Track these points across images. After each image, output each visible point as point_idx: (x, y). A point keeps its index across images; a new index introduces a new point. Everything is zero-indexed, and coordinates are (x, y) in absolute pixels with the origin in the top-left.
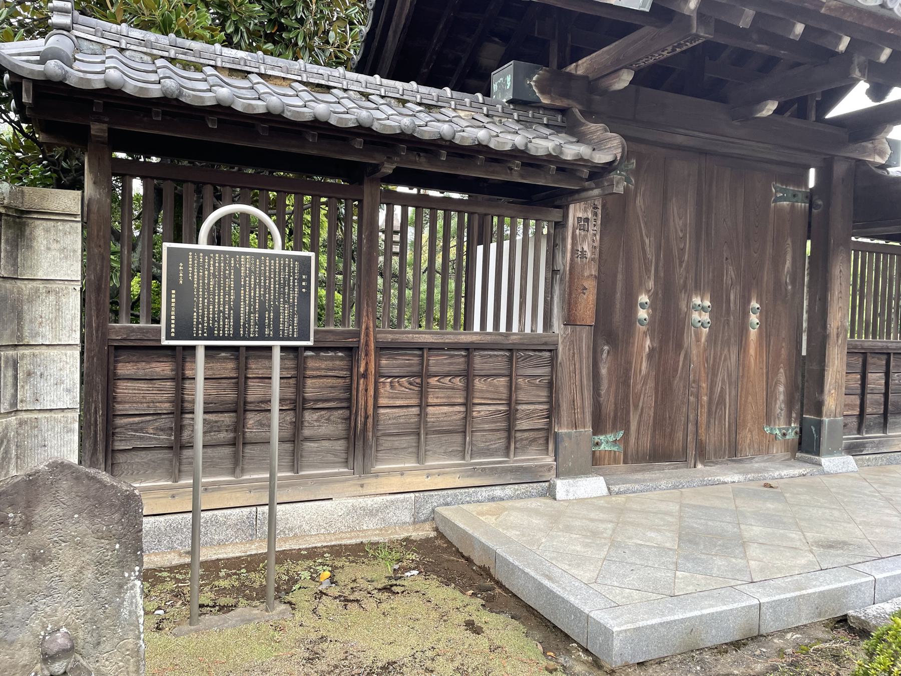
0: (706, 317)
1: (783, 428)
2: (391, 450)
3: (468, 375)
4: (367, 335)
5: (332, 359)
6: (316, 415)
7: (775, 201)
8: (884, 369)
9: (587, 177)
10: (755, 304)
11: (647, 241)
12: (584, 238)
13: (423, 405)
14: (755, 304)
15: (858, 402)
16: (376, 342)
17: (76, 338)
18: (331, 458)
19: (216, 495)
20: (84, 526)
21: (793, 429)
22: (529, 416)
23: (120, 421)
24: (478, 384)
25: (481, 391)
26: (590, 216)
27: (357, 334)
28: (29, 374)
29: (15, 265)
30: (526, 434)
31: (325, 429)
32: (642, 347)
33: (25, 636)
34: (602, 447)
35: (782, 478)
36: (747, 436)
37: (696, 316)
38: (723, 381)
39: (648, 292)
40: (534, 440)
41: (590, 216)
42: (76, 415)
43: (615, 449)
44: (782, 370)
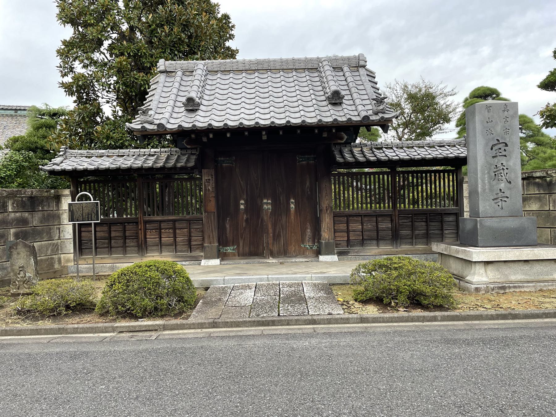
0: (270, 206)
2: (151, 250)
3: (175, 229)
4: (140, 218)
5: (132, 225)
6: (129, 241)
7: (299, 162)
8: (361, 222)
9: (361, 129)
11: (242, 183)
12: (209, 185)
13: (160, 238)
15: (346, 235)
16: (143, 220)
18: (134, 252)
19: (104, 260)
20: (24, 249)
21: (316, 246)
22: (196, 241)
23: (83, 242)
24: (177, 231)
25: (179, 233)
26: (210, 178)
28: (62, 231)
29: (58, 207)
30: (195, 246)
31: (132, 244)
32: (243, 217)
33: (17, 265)
34: (229, 251)
36: (292, 248)
38: (279, 228)
39: (244, 199)
40: (198, 248)
41: (210, 178)
42: (72, 240)
43: (234, 251)
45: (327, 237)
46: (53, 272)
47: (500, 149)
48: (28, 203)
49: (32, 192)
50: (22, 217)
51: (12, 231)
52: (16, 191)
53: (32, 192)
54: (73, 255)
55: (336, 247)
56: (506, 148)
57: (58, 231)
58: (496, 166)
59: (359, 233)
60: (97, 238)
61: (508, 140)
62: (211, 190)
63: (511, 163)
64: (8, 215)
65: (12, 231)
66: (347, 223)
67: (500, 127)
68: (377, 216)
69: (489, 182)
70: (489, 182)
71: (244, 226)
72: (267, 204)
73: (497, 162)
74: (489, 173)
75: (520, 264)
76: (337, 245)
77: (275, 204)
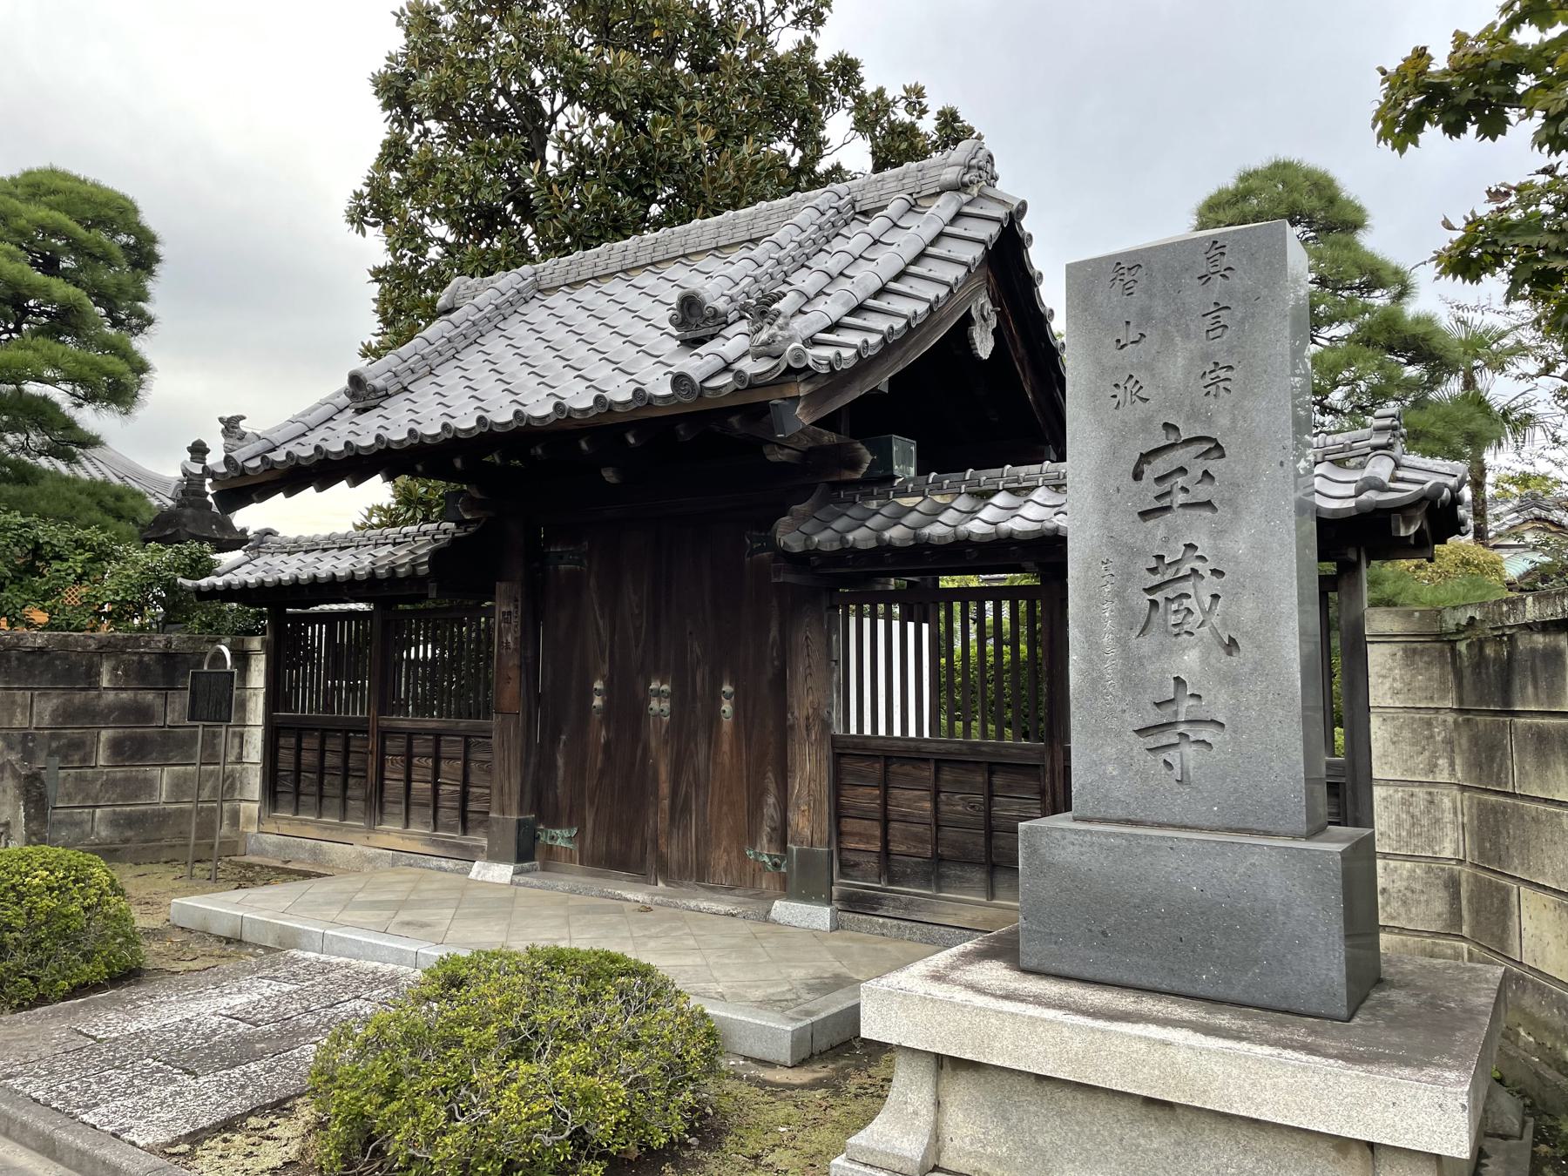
0: (666, 705)
1: (776, 856)
7: (751, 555)
10: (727, 688)
13: (409, 781)
14: (727, 688)
15: (878, 833)
17: (1378, 792)
19: (307, 828)
27: (368, 719)
35: (700, 911)
36: (720, 858)
37: (654, 704)
39: (602, 678)
41: (512, 609)
42: (259, 767)
43: (570, 846)
44: (770, 775)
45: (807, 832)
46: (207, 844)
47: (1182, 470)
48: (158, 670)
49: (169, 642)
50: (136, 701)
51: (105, 735)
52: (124, 639)
53: (169, 642)
54: (257, 806)
55: (843, 875)
56: (1213, 465)
57: (237, 741)
58: (1160, 558)
59: (920, 829)
60: (303, 767)
61: (1224, 421)
62: (512, 645)
63: (1240, 544)
64: (99, 696)
65: (105, 735)
66: (886, 788)
67: (1181, 362)
68: (992, 768)
69: (1122, 643)
70: (1118, 640)
71: (599, 765)
72: (658, 694)
73: (1166, 540)
74: (1119, 594)
75: (1122, 1110)
76: (846, 868)
77: (681, 699)
